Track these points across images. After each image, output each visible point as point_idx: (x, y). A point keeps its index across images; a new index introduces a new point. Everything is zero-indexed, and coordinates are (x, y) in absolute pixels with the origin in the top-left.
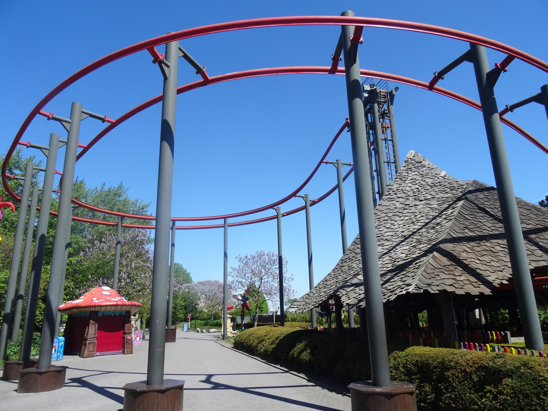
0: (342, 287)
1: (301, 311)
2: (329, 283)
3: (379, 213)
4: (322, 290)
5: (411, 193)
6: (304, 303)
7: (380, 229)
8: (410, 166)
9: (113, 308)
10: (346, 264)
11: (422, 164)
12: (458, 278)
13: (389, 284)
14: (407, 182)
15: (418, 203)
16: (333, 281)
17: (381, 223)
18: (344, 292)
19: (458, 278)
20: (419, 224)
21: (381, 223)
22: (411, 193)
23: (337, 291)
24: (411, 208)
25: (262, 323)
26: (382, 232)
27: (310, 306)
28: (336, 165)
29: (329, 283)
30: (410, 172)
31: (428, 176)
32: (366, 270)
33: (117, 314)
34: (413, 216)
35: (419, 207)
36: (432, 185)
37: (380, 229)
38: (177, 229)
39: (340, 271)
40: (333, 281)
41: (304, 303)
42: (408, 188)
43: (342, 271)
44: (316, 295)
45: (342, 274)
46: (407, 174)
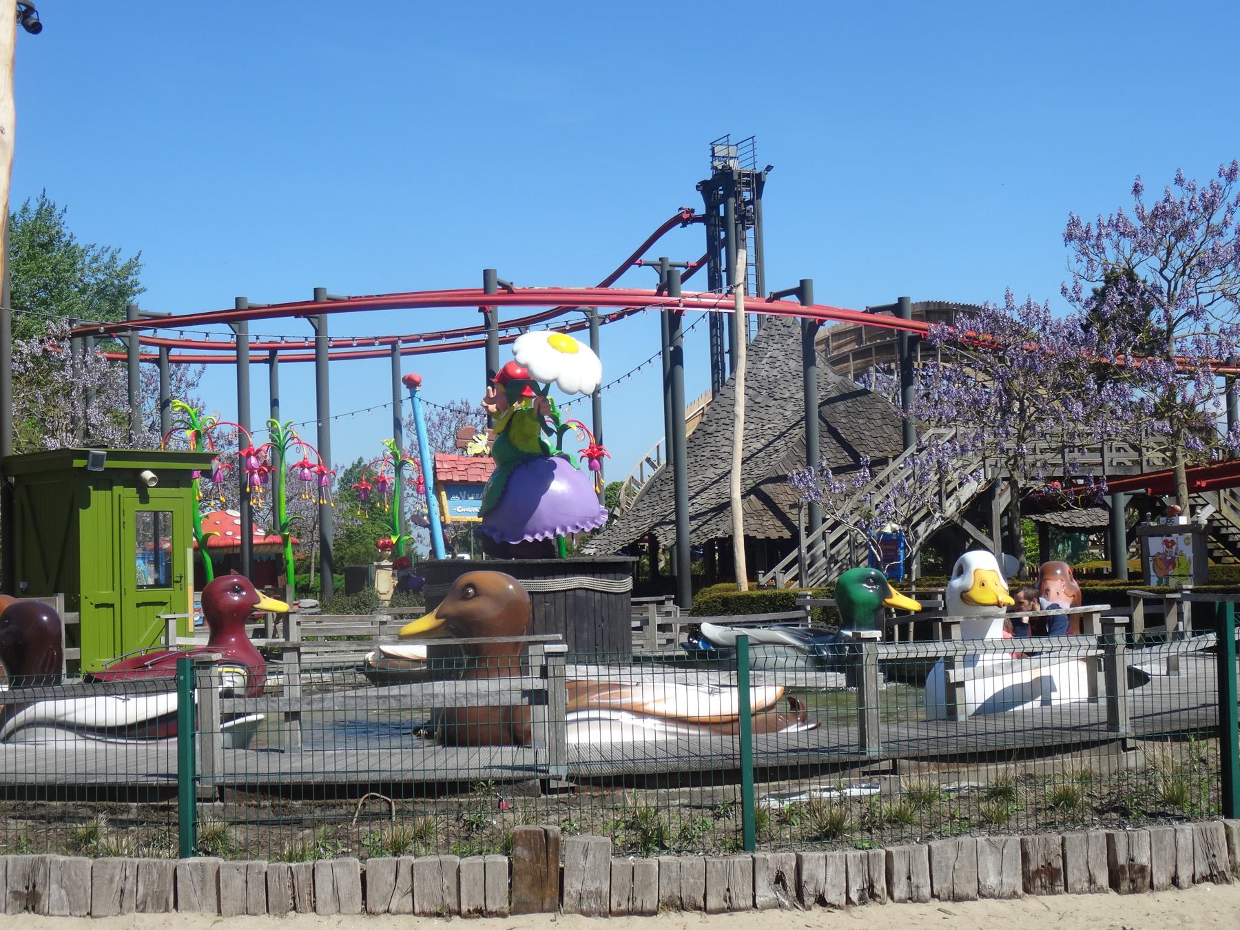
0: (660, 524)
1: (603, 552)
2: (642, 514)
3: (719, 409)
4: (633, 524)
5: (765, 384)
6: (606, 542)
7: (717, 439)
8: (773, 332)
9: (268, 548)
10: (667, 488)
11: (790, 330)
12: (765, 523)
13: (706, 526)
14: (764, 362)
15: (772, 403)
16: (647, 512)
17: (719, 429)
18: (661, 531)
19: (765, 523)
20: (763, 441)
21: (719, 429)
22: (765, 384)
23: (653, 528)
24: (761, 410)
25: (527, 561)
26: (719, 444)
27: (616, 546)
28: (659, 268)
29: (642, 514)
30: (771, 343)
31: (793, 356)
32: (677, 510)
33: (265, 559)
34: (759, 426)
35: (771, 411)
36: (794, 373)
37: (717, 439)
38: (280, 361)
39: (658, 498)
40: (647, 512)
41: (606, 542)
42: (763, 373)
43: (661, 499)
44: (624, 530)
45: (660, 502)
46: (766, 346)
